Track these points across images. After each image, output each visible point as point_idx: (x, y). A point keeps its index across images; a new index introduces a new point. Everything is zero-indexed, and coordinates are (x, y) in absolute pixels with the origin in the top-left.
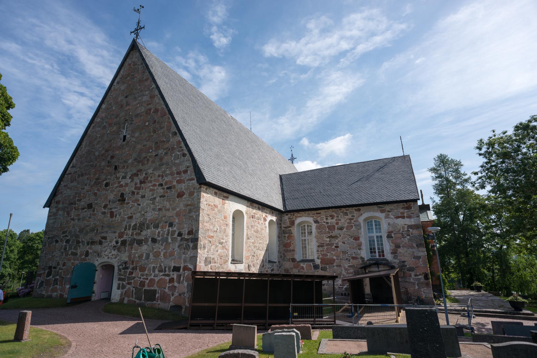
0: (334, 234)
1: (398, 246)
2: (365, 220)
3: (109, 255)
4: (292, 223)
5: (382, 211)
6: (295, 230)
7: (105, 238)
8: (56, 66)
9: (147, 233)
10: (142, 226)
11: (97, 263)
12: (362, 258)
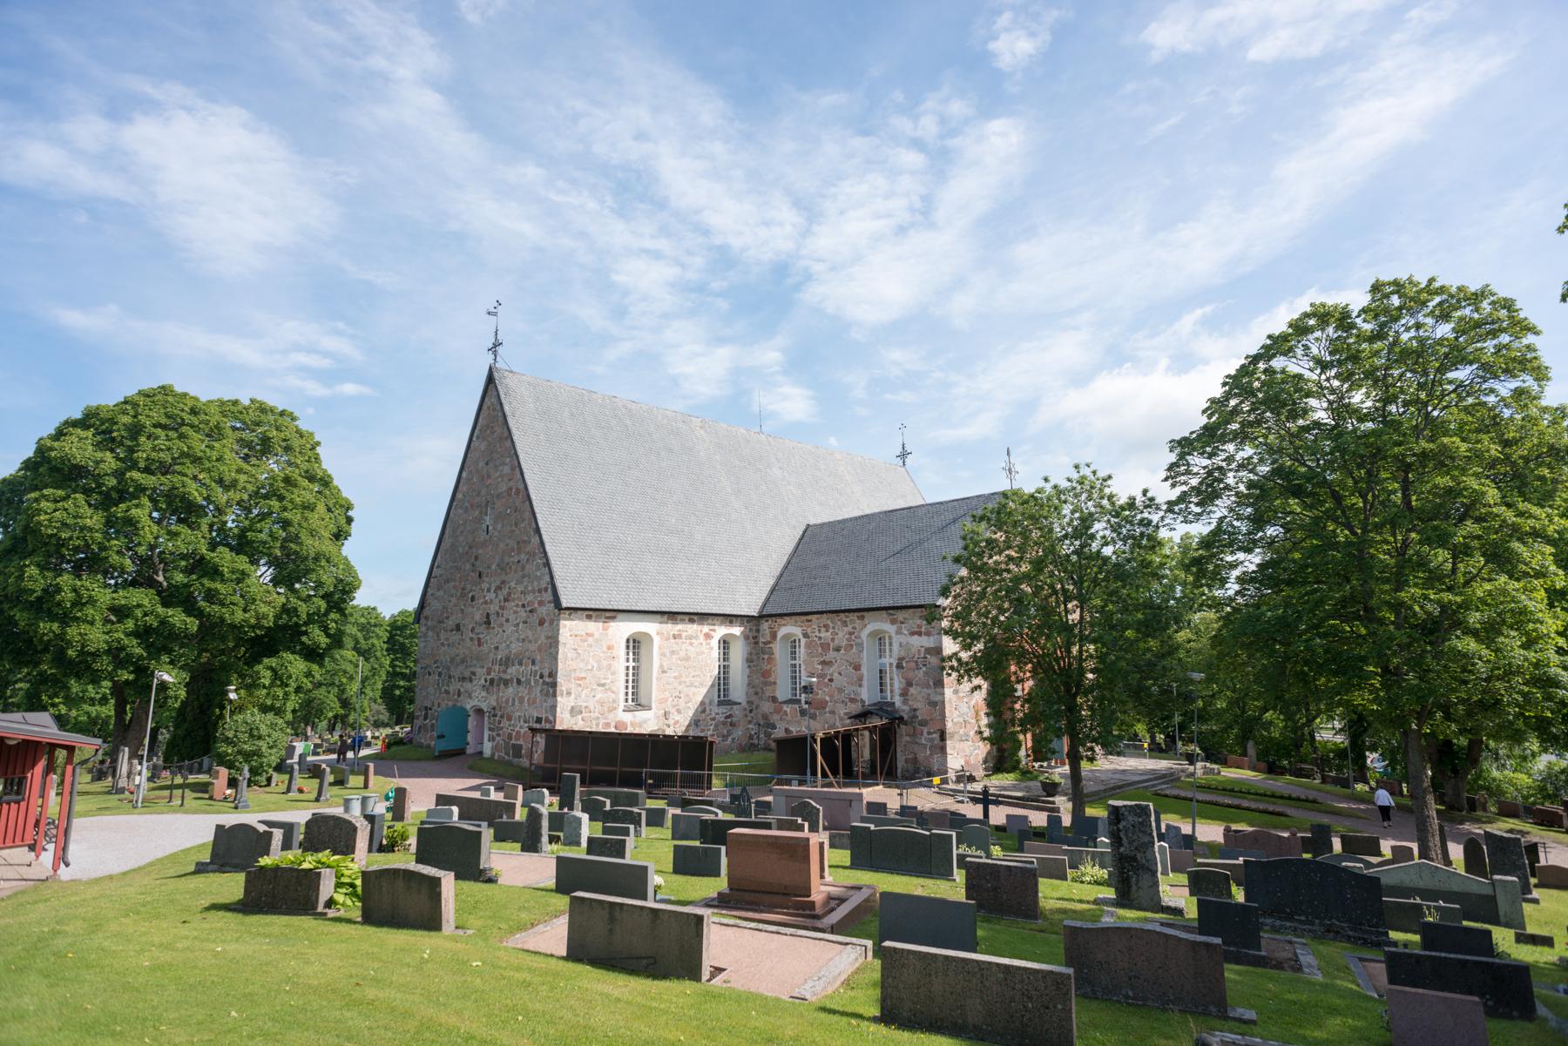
0: (827, 658)
1: (909, 684)
2: (873, 634)
3: (478, 698)
4: (774, 635)
5: (893, 622)
6: (778, 649)
7: (474, 673)
8: (609, 200)
9: (513, 671)
10: (507, 662)
11: (468, 707)
12: (863, 701)
